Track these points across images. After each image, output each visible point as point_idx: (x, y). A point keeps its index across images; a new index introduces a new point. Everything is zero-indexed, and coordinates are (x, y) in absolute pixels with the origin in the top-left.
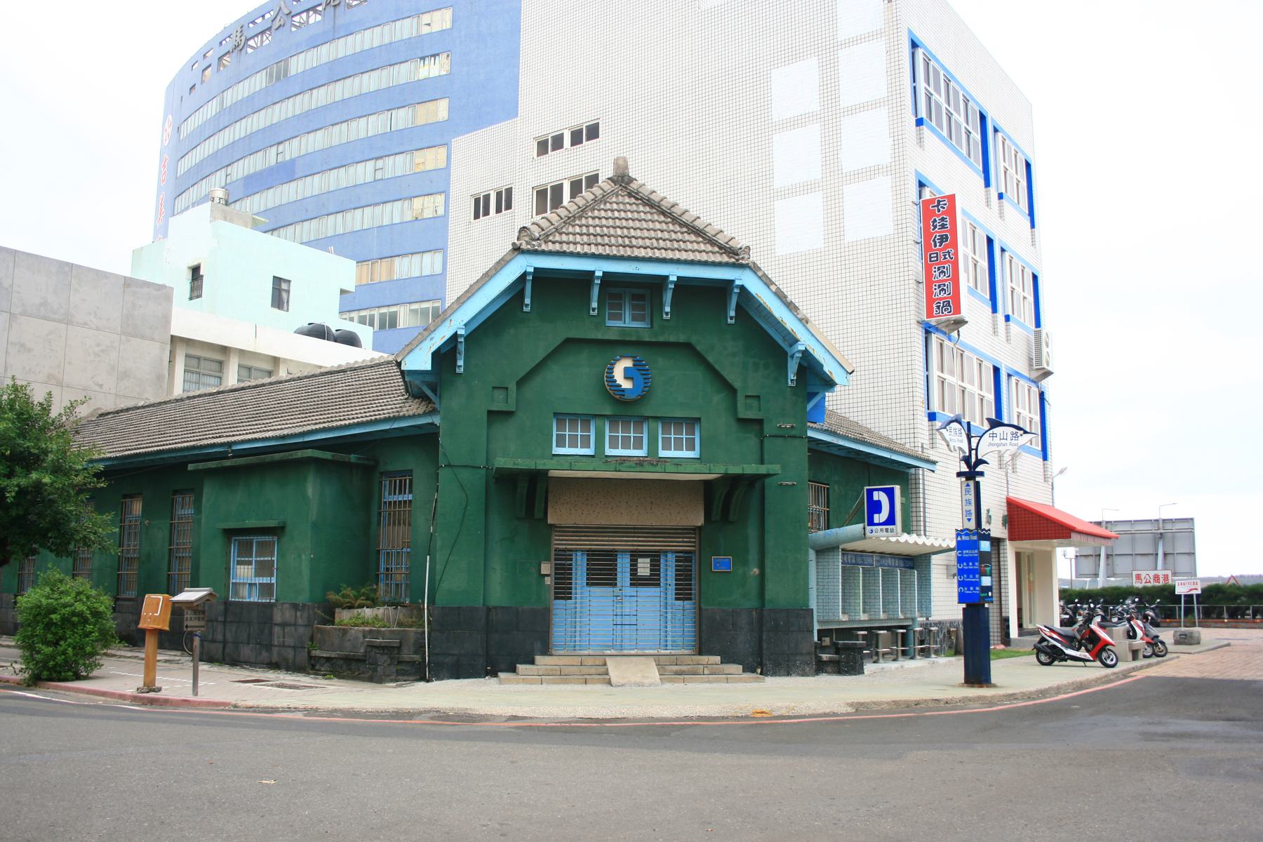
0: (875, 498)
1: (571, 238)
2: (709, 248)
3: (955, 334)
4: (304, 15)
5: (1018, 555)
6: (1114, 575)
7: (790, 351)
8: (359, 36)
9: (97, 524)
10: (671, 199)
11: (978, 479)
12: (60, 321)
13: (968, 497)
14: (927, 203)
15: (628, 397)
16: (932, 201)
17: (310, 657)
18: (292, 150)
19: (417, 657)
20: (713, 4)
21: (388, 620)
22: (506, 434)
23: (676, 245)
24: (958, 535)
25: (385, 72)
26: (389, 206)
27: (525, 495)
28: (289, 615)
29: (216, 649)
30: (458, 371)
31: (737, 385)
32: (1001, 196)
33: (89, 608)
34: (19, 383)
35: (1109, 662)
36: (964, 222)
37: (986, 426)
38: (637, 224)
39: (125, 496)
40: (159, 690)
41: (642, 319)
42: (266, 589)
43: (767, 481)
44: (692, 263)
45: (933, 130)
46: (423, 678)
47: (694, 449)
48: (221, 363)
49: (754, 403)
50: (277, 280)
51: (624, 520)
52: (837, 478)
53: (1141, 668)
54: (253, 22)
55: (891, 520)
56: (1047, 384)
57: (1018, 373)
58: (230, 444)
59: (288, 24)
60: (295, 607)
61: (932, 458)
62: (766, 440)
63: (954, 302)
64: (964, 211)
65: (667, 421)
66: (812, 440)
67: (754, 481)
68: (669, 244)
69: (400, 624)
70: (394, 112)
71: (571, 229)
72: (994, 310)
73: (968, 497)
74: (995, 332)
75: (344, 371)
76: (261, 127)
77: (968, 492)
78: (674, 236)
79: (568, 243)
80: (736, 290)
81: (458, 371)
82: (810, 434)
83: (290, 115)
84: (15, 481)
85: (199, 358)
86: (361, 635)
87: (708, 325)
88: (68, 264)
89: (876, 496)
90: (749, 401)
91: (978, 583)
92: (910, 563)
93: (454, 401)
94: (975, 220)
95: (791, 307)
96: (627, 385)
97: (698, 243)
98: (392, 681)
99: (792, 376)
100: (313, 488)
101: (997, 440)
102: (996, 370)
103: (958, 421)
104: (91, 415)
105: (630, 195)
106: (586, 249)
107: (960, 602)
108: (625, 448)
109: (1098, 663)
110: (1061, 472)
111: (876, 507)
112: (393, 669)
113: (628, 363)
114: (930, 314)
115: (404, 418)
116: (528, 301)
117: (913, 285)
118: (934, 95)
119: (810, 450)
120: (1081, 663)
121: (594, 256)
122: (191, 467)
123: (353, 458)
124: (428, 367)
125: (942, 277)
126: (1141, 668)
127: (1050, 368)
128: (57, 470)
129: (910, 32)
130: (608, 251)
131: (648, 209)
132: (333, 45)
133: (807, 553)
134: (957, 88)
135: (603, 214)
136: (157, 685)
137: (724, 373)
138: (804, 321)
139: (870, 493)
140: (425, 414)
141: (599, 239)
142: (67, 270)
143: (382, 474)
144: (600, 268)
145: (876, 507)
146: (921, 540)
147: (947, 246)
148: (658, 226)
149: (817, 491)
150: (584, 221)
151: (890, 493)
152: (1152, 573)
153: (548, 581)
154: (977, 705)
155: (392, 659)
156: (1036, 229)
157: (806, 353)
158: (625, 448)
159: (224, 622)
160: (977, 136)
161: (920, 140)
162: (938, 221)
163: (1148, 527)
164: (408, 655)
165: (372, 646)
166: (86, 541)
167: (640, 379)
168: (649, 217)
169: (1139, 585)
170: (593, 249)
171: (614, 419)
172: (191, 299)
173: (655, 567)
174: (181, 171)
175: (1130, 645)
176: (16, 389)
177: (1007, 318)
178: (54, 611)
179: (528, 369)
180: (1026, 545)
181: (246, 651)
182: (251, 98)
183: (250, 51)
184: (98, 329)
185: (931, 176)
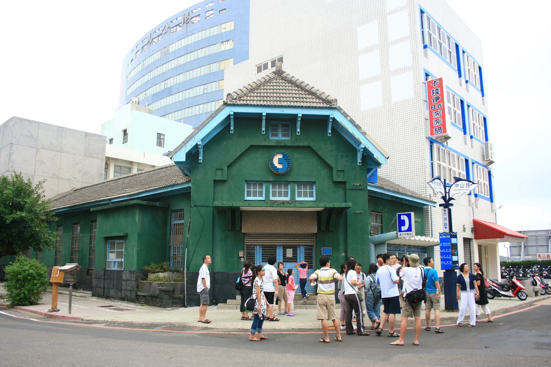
0: (402, 218)
1: (252, 98)
2: (318, 101)
3: (445, 143)
4: (175, 28)
5: (480, 247)
6: (528, 255)
7: (358, 148)
8: (197, 35)
9: (56, 237)
10: (301, 80)
11: (450, 207)
12: (58, 151)
13: (445, 216)
14: (429, 83)
15: (280, 172)
16: (432, 81)
17: (137, 295)
18: (170, 83)
19: (181, 296)
20: (339, 10)
21: (169, 278)
22: (223, 190)
23: (302, 100)
24: (440, 235)
25: (207, 49)
26: (210, 103)
27: (231, 219)
28: (128, 275)
29: (101, 291)
30: (199, 162)
31: (333, 165)
32: (467, 82)
33: (36, 272)
34: (18, 174)
35: (522, 298)
36: (448, 93)
37: (453, 180)
38: (284, 91)
39: (74, 224)
40: (59, 310)
41: (287, 136)
42: (120, 264)
43: (348, 210)
44: (309, 108)
45: (432, 50)
46: (184, 306)
47: (313, 197)
48: (130, 168)
49: (342, 174)
50: (159, 135)
51: (278, 230)
52: (386, 210)
53: (540, 300)
54: (155, 32)
55: (410, 229)
56: (492, 167)
57: (477, 162)
58: (110, 199)
59: (169, 32)
60: (131, 272)
61: (434, 201)
62: (347, 192)
63: (443, 128)
64: (447, 87)
65: (300, 184)
66: (370, 191)
67: (341, 211)
68: (298, 99)
69: (175, 280)
70: (211, 65)
71: (252, 94)
72: (465, 133)
73: (445, 216)
74: (466, 143)
75: (167, 167)
76: (159, 74)
77: (445, 214)
78: (301, 96)
79: (250, 100)
80: (331, 120)
81: (199, 162)
82: (369, 188)
83: (170, 68)
84: (12, 215)
85: (120, 167)
86: (157, 285)
87: (317, 137)
88: (61, 127)
89: (403, 217)
90: (339, 173)
91: (451, 260)
92: (424, 250)
93: (198, 176)
94: (454, 92)
95: (357, 127)
96: (279, 166)
97: (313, 99)
98: (170, 307)
99: (359, 161)
100: (137, 217)
101: (459, 188)
102: (467, 161)
103: (439, 178)
104: (71, 190)
105: (282, 79)
106: (258, 103)
107: (442, 269)
108: (280, 196)
109: (517, 298)
110: (500, 208)
111: (402, 223)
112: (171, 301)
113: (280, 156)
114: (432, 134)
115: (178, 185)
116: (232, 128)
117: (423, 120)
118: (428, 32)
119: (369, 196)
120: (508, 298)
121: (262, 106)
122: (91, 210)
123: (157, 204)
124: (184, 160)
125: (437, 116)
126: (540, 300)
127: (493, 160)
128: (30, 211)
129: (419, 6)
130: (268, 103)
131: (290, 85)
132: (186, 39)
133: (369, 245)
134: (444, 32)
135: (269, 87)
136: (58, 308)
137: (326, 160)
138: (364, 134)
139: (400, 216)
140: (187, 182)
141: (265, 98)
142: (61, 130)
143: (172, 211)
144: (264, 111)
145: (402, 223)
146: (427, 239)
147: (439, 102)
148: (294, 92)
149: (376, 216)
150: (259, 91)
151: (409, 216)
152: (546, 254)
153: (242, 260)
154: (449, 322)
155: (170, 296)
156: (484, 97)
157: (365, 149)
158: (280, 196)
159: (104, 279)
160: (454, 54)
161: (426, 55)
162: (435, 91)
163: (543, 233)
164: (177, 295)
165: (161, 291)
166: (46, 242)
167: (286, 163)
168: (290, 88)
169: (540, 260)
170: (262, 103)
171: (274, 183)
172: (123, 143)
173: (295, 253)
174: (128, 94)
175: (534, 289)
176: (17, 177)
177: (471, 137)
178: (20, 274)
179: (232, 160)
180: (483, 242)
181: (112, 292)
182: (154, 62)
183: (154, 43)
184: (74, 154)
185: (431, 71)
